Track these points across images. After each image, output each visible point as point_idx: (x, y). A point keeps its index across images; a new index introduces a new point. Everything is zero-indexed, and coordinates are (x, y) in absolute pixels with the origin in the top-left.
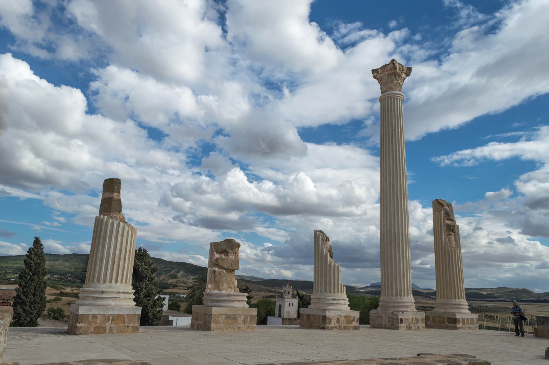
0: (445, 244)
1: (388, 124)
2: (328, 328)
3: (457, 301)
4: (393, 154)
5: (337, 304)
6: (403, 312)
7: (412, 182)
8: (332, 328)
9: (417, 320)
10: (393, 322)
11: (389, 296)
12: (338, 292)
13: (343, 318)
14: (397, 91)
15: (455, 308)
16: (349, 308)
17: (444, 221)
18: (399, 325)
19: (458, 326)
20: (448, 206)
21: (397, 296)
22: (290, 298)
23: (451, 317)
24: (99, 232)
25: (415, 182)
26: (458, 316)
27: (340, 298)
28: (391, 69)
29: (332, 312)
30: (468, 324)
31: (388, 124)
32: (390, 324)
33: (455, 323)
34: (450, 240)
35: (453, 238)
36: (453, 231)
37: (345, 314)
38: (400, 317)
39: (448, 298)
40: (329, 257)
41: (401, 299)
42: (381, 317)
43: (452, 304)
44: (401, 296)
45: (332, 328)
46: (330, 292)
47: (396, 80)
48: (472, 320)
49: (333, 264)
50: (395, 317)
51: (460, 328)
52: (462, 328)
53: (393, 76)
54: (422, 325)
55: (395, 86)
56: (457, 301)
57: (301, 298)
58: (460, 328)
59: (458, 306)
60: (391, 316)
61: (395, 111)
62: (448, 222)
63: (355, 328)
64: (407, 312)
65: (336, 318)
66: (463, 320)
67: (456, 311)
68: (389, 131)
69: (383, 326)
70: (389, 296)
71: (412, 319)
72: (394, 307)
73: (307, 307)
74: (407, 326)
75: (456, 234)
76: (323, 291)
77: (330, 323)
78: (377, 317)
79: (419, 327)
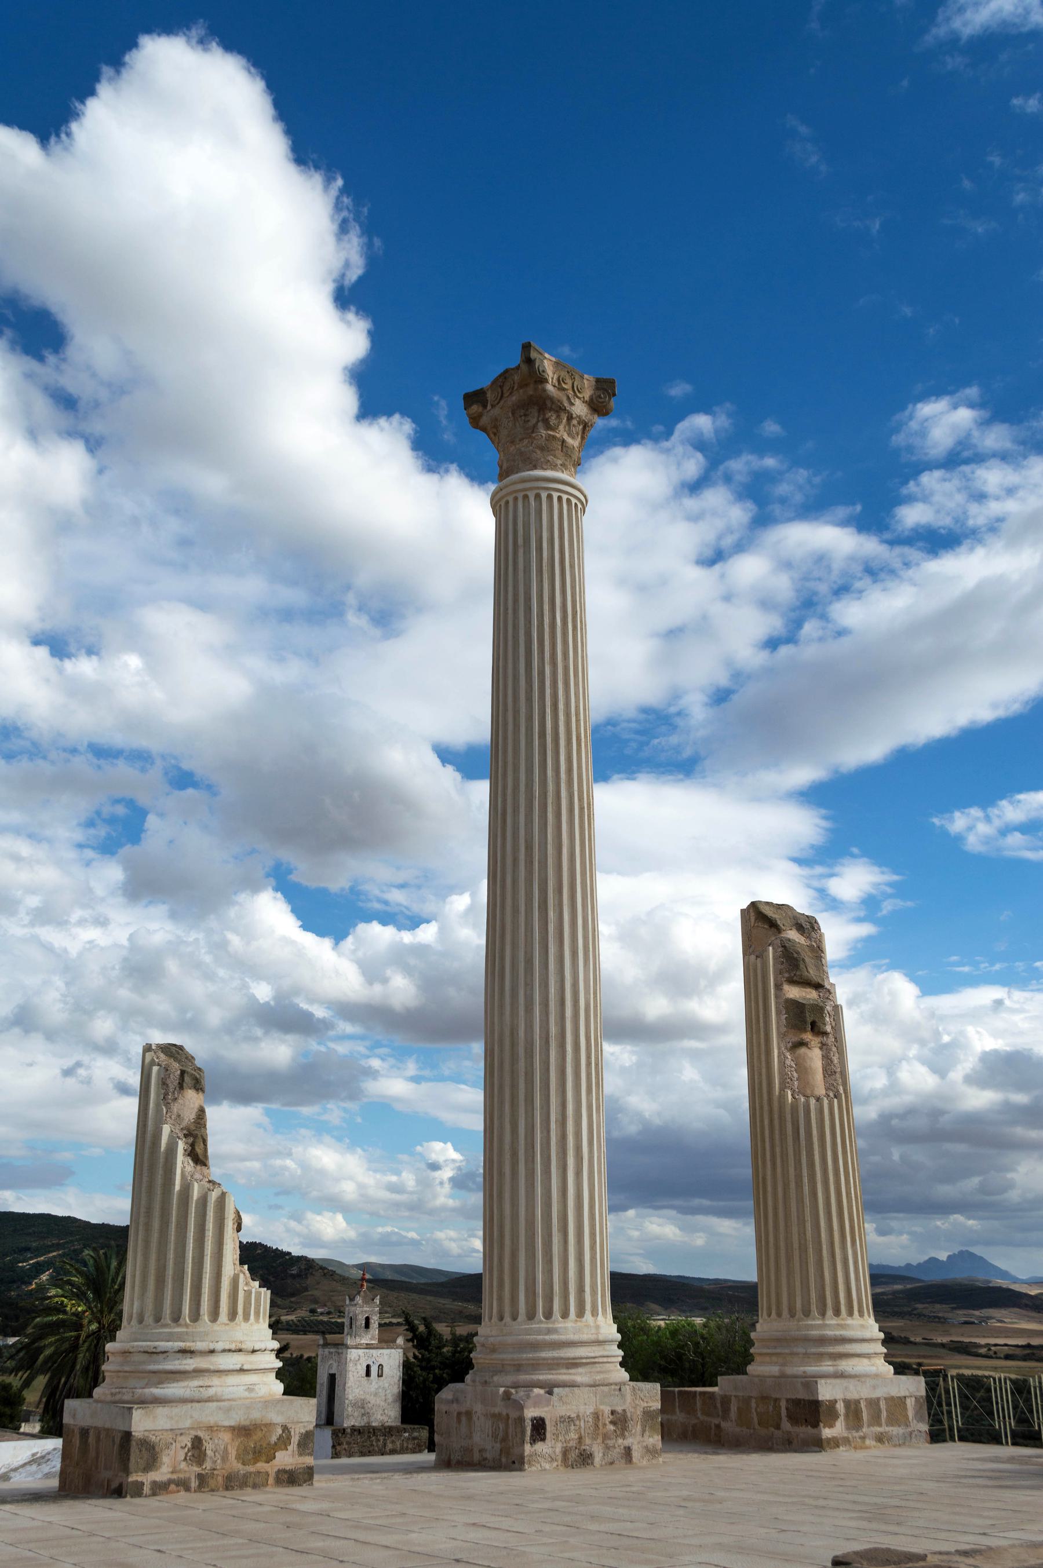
0: (782, 1089)
1: (516, 601)
2: (137, 1491)
3: (831, 1325)
4: (530, 718)
5: (198, 1372)
6: (550, 1388)
7: (900, 903)
8: (159, 1488)
9: (620, 1421)
10: (505, 1439)
11: (141, 1321)
12: (851, 1313)
13: (226, 1437)
14: (554, 467)
15: (821, 1356)
16: (279, 1387)
17: (778, 987)
18: (528, 1448)
19: (827, 1433)
20: (800, 928)
21: (531, 1316)
22: (369, 1347)
23: (802, 1395)
24: (150, 1164)
25: (909, 904)
26: (826, 1391)
27: (219, 1346)
28: (523, 385)
29: (161, 1411)
30: (876, 1420)
31: (516, 601)
32: (498, 1446)
33: (815, 1425)
34: (802, 1069)
35: (814, 1057)
36: (816, 1029)
37: (236, 1418)
38: (530, 1413)
39: (792, 1314)
40: (181, 1160)
41: (555, 1331)
42: (469, 1414)
43: (807, 1340)
44: (548, 1315)
45: (159, 1488)
46: (176, 1318)
47: (549, 427)
48: (897, 1404)
49: (196, 1193)
50: (514, 1415)
51: (835, 1443)
52: (847, 1441)
53: (534, 411)
54: (644, 1439)
55: (542, 449)
56: (831, 1325)
57: (422, 1341)
58: (835, 1443)
59: (832, 1347)
60: (500, 1408)
61: (540, 549)
62: (793, 992)
63: (290, 1478)
64: (573, 1385)
65: (186, 1440)
66: (853, 1409)
67: (827, 1367)
68: (515, 627)
69: (476, 1457)
70: (501, 1318)
71: (596, 1416)
72: (518, 1368)
73: (90, 1396)
74: (565, 1453)
75: (831, 1039)
76: (149, 1319)
77: (152, 1462)
78: (459, 1414)
79: (628, 1452)
